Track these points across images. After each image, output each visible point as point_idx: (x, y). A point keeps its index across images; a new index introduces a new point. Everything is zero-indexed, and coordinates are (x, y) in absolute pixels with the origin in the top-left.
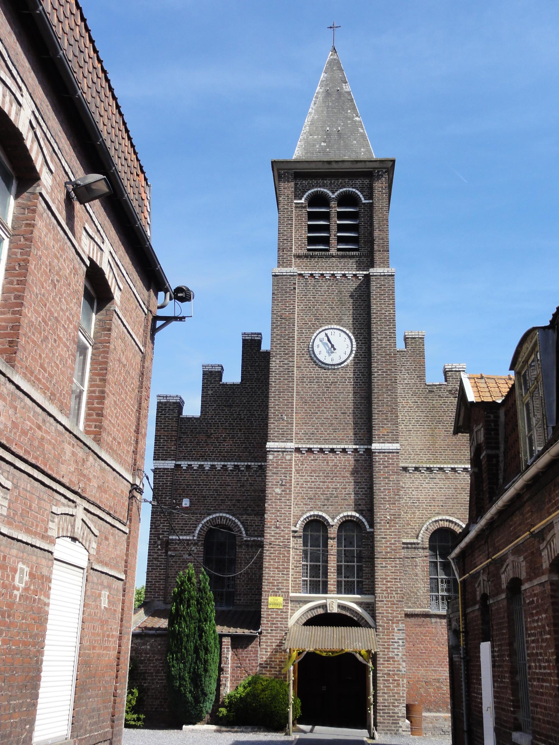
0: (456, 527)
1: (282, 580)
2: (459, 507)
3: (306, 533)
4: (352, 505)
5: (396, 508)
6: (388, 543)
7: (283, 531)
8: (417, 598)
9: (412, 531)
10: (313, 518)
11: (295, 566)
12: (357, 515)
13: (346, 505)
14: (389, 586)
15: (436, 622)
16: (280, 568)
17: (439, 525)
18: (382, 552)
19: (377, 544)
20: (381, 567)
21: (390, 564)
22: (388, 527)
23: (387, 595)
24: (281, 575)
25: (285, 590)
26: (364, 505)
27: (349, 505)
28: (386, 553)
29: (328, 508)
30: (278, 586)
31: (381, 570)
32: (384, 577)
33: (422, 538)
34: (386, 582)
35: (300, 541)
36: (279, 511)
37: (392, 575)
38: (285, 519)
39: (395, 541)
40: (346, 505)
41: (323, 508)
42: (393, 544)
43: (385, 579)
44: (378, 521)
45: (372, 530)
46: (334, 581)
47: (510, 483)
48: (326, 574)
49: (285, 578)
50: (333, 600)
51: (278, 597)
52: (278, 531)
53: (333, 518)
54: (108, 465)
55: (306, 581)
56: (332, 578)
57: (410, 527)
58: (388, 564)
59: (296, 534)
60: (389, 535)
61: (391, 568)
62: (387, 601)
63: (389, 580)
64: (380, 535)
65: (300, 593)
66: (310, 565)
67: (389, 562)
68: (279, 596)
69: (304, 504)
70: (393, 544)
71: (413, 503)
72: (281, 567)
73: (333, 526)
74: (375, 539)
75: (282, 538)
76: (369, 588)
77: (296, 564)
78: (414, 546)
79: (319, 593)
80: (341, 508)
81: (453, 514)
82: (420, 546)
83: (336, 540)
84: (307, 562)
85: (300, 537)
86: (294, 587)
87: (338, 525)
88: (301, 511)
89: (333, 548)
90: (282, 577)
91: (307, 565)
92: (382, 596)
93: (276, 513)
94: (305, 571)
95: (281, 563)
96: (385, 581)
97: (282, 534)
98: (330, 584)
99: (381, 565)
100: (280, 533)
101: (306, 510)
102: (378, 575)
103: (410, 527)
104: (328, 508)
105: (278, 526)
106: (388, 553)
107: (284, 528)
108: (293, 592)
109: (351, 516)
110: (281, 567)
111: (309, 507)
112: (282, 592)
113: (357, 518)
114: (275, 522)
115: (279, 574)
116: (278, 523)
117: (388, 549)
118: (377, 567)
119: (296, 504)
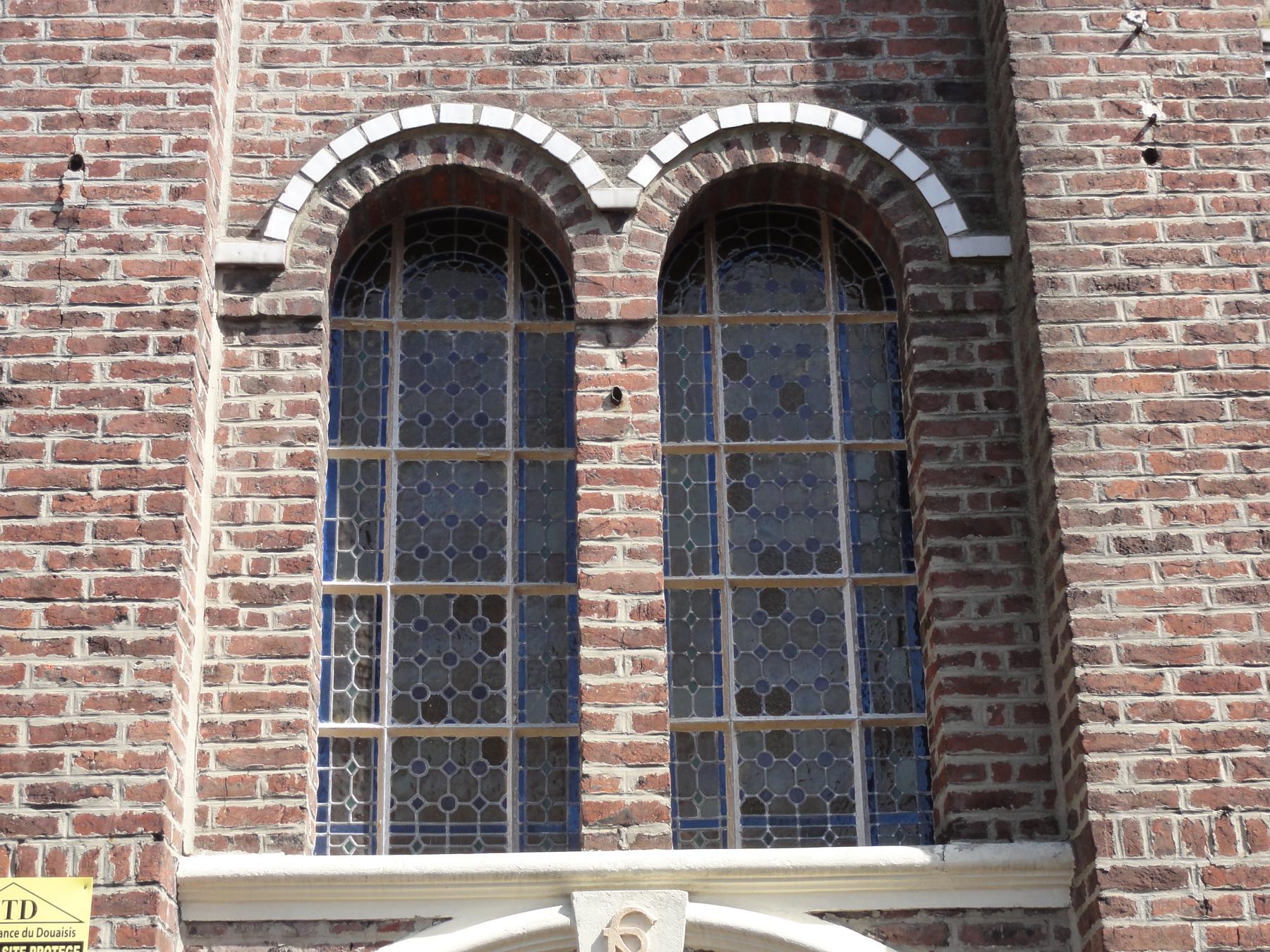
1: (95, 703)
3: (361, 322)
4: (788, 51)
5: (1220, 35)
6: (1174, 329)
7: (120, 245)
10: (422, 161)
11: (238, 593)
12: (850, 125)
13: (741, 52)
14: (1221, 722)
16: (72, 588)
18: (1122, 412)
19: (1056, 344)
20: (1124, 547)
21: (1207, 515)
22: (1153, 191)
23: (1206, 817)
24: (81, 657)
25: (115, 806)
26: (898, 48)
27: (765, 54)
28: (1159, 414)
29: (566, 79)
30: (44, 764)
31: (1123, 574)
32: (1160, 636)
34: (1191, 684)
35: (308, 362)
36: (88, 77)
37: (1241, 624)
38: (151, 147)
39: (1239, 307)
40: (741, 52)
41: (521, 79)
42: (1221, 335)
43: (1175, 656)
44: (1060, 136)
45: (994, 245)
46: (641, 723)
48: (557, 678)
49: (127, 684)
50: (638, 901)
51: (38, 885)
52: (70, 247)
53: (618, 163)
54: (51, 944)
55: (366, 747)
56: (625, 696)
58: (1187, 514)
59: (258, 304)
60: (1174, 257)
61: (1220, 554)
62: (1208, 878)
63: (1211, 664)
64: (1086, 260)
65: (292, 845)
66: (405, 604)
67: (1194, 499)
68: (54, 867)
69: (338, 54)
70: (1221, 335)
72: (86, 579)
73: (618, 216)
74: (1045, 298)
75: (110, 314)
76: (1002, 772)
77: (259, 569)
79: (495, 843)
80: (693, 77)
83: (649, 346)
84: (372, 569)
85: (306, 323)
86: (223, 791)
87: (667, 217)
88: (310, 107)
89: (625, 411)
90: (91, 674)
91: (371, 605)
92: (1159, 828)
93: (64, 98)
94: (355, 656)
95: (89, 545)
96: (1171, 678)
97: (110, 279)
98: (608, 754)
99: (1126, 531)
100: (87, 272)
101: (358, 96)
102: (1098, 628)
104: (566, 79)
105: (73, 199)
106: (1183, 415)
107: (134, 218)
108: (218, 844)
109: (792, 133)
110: (86, 579)
111: (394, 72)
112: (86, 825)
113: (852, 146)
114: (43, 171)
115: (62, 648)
116: (75, 182)
117: (1180, 378)
118: (1083, 544)
119: (271, 55)
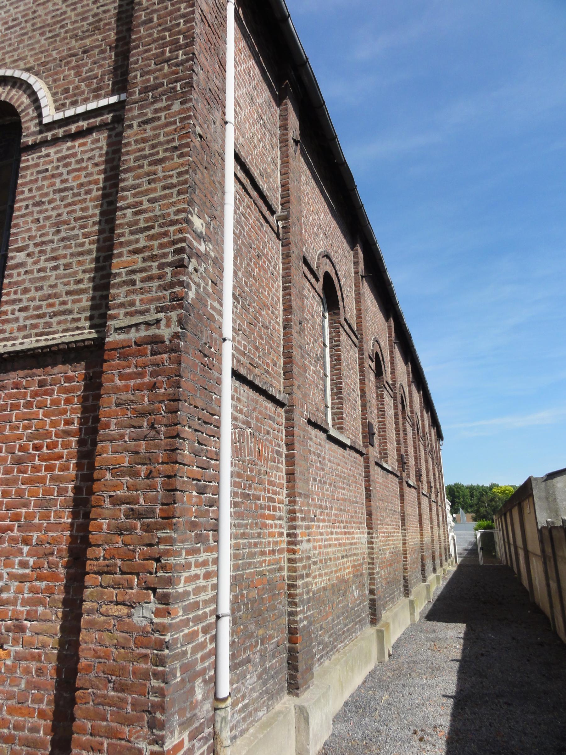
0: (14, 92)
2: (38, 37)
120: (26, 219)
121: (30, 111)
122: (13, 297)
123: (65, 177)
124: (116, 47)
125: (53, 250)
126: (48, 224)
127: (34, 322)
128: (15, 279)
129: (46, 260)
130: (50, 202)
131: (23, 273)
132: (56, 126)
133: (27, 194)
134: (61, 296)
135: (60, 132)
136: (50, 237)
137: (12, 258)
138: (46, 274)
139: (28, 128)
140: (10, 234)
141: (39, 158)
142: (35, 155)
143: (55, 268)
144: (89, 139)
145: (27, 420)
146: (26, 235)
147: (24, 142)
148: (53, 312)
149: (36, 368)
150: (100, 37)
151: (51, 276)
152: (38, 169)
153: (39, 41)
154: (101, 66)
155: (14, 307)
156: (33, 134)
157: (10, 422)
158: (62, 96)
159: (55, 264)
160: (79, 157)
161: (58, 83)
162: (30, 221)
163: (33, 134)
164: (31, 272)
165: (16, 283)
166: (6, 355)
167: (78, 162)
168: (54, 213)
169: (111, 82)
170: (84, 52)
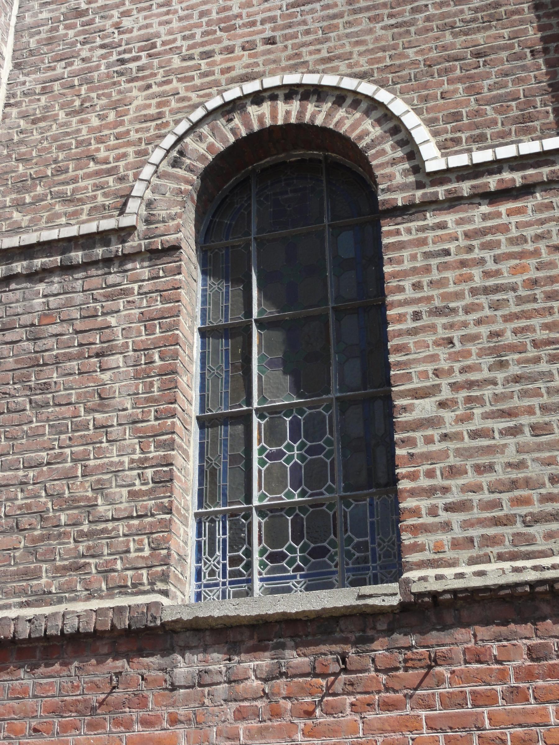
0: (341, 113)
2: (365, 25)
8: (90, 535)
9: (98, 187)
15: (202, 681)
17: (247, 123)
33: (150, 204)
47: (263, 532)
57: (92, 167)
71: (122, 61)
78: (99, 252)
81: (330, 60)
82: (133, 243)
103: (92, 167)
120: (420, 337)
121: (387, 146)
122: (424, 482)
123: (491, 266)
124: (546, 51)
125: (497, 398)
126: (473, 348)
127: (491, 531)
128: (421, 448)
129: (486, 416)
130: (467, 310)
131: (437, 438)
132: (453, 176)
133: (409, 293)
134: (543, 485)
135: (465, 188)
136: (485, 374)
137: (405, 409)
138: (492, 442)
139: (390, 177)
140: (389, 364)
141: (423, 229)
142: (413, 225)
143: (515, 431)
144: (529, 203)
145: (520, 726)
146: (430, 368)
147: (385, 202)
148: (531, 514)
149: (516, 623)
150: (505, 32)
151: (505, 445)
152: (426, 249)
153: (371, 31)
154: (519, 81)
155: (434, 502)
156: (403, 188)
157: (479, 729)
158: (449, 126)
159: (511, 424)
160: (514, 233)
161: (432, 104)
162: (430, 343)
163: (403, 188)
164: (457, 436)
165: (427, 457)
166: (448, 596)
167: (512, 241)
168: (484, 330)
169: (550, 109)
170: (478, 55)
